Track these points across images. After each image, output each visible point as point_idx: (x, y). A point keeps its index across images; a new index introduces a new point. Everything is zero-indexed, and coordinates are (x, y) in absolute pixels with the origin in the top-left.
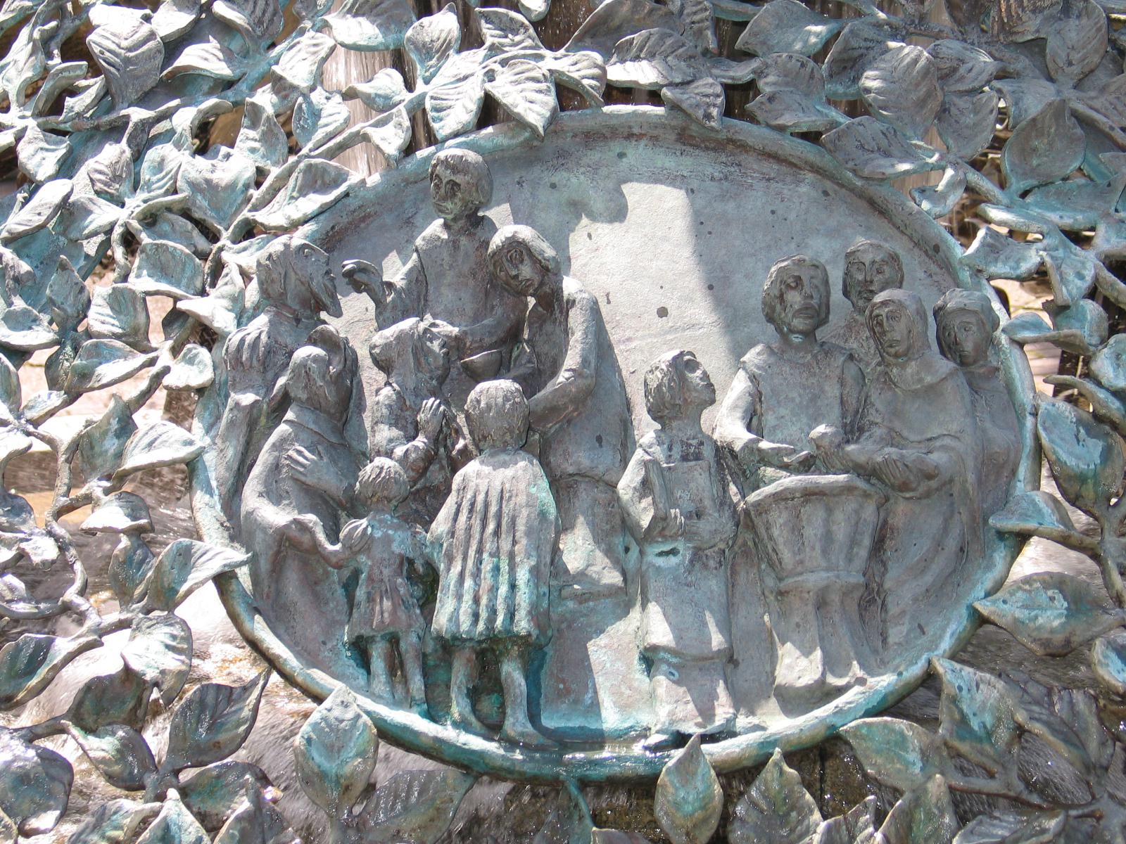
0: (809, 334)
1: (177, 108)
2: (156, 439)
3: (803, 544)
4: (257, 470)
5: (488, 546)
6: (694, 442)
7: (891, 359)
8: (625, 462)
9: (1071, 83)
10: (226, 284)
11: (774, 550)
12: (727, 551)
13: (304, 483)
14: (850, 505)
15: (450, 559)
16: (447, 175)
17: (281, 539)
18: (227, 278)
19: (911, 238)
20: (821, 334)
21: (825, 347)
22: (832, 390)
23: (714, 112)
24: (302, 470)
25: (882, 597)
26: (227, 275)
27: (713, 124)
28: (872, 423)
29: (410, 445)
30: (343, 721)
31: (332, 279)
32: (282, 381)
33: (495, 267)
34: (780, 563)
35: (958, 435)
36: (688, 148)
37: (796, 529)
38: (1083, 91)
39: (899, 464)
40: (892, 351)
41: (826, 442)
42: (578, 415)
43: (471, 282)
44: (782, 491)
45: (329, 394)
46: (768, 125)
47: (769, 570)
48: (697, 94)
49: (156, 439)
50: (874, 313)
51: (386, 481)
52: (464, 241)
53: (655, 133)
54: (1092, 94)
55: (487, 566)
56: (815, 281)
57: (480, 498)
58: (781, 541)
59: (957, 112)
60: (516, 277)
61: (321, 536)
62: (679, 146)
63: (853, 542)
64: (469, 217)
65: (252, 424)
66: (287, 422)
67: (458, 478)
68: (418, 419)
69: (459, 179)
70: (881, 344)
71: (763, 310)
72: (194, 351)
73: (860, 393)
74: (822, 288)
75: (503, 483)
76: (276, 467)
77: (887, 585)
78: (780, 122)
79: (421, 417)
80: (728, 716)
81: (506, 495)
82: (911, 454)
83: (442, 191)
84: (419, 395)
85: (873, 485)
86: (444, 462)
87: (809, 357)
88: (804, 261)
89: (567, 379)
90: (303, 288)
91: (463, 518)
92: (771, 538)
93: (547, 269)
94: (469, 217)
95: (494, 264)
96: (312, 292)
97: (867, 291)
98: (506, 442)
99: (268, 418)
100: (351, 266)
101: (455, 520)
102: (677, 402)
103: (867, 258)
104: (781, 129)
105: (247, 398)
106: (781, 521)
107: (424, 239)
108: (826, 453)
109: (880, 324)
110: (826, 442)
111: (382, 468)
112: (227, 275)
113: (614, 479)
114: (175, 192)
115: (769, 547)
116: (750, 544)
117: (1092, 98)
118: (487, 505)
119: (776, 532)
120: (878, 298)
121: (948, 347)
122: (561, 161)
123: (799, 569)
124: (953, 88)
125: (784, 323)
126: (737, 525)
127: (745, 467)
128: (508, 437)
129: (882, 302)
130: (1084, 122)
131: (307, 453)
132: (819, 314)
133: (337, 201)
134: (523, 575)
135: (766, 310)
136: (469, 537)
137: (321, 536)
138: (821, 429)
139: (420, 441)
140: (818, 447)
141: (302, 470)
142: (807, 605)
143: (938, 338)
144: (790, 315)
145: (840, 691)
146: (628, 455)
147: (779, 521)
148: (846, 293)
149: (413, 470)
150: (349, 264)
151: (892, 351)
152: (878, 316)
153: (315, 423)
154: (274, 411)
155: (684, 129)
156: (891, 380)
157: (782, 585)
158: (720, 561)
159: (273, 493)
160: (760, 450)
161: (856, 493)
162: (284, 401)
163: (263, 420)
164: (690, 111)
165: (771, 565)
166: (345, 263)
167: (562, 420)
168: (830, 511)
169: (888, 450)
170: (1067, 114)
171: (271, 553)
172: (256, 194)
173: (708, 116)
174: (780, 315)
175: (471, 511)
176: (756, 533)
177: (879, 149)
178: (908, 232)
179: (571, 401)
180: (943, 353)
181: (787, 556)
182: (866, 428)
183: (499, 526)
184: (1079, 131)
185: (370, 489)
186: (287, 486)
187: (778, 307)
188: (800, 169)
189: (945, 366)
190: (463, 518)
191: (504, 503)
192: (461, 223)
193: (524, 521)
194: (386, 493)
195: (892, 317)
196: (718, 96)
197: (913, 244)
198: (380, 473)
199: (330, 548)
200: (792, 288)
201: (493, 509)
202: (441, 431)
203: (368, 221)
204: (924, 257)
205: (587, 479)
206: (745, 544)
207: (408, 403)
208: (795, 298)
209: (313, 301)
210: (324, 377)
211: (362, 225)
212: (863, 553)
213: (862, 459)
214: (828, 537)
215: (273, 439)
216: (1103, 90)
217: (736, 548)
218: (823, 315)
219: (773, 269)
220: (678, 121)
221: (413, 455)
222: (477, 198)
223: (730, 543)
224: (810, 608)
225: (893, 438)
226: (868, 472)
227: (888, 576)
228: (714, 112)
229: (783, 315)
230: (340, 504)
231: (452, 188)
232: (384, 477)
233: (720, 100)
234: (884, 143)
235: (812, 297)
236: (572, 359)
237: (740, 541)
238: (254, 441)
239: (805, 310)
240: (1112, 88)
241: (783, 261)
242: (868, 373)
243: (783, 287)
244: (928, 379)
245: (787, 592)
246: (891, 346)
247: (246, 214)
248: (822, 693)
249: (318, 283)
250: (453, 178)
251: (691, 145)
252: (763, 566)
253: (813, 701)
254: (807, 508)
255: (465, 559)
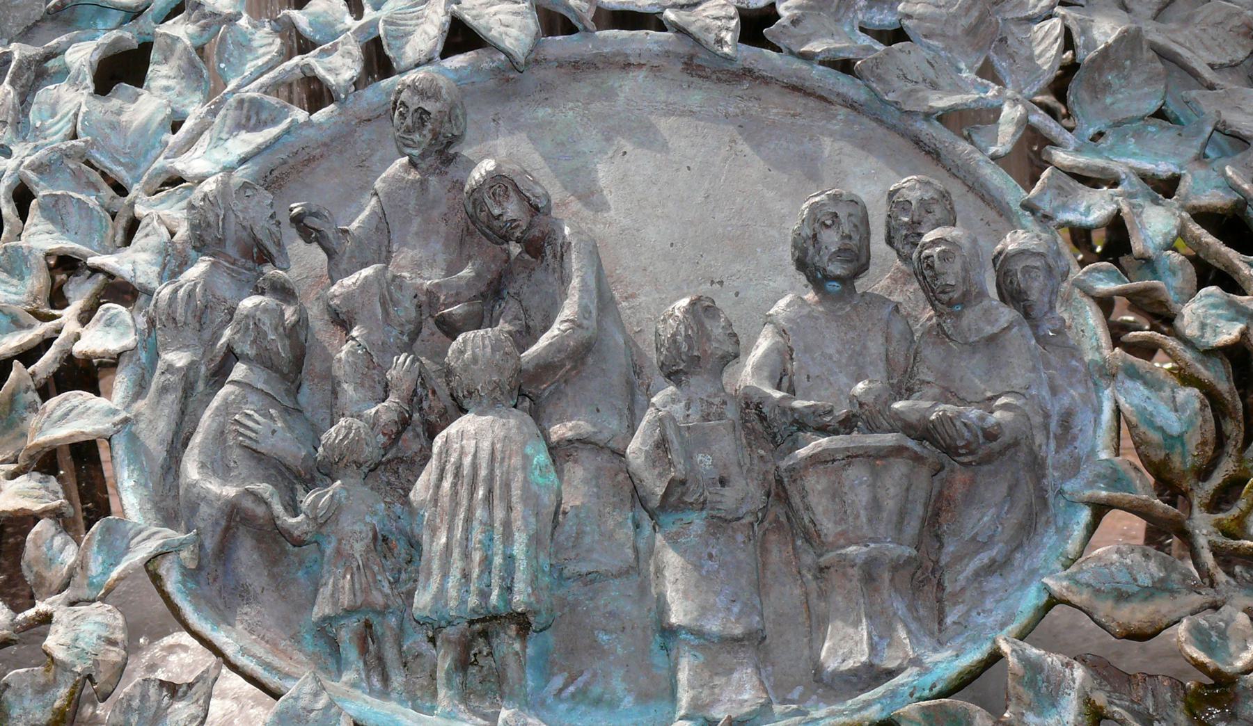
0: (847, 281)
1: (70, 43)
2: (71, 411)
3: (845, 512)
4: (197, 439)
5: (479, 513)
6: (717, 401)
7: (944, 307)
8: (632, 429)
9: (1150, 13)
10: (147, 235)
11: (812, 521)
12: (756, 525)
13: (255, 451)
14: (899, 468)
15: (434, 531)
16: (415, 102)
17: (232, 512)
18: (149, 229)
19: (964, 183)
20: (861, 285)
21: (867, 298)
22: (875, 346)
23: (728, 37)
24: (253, 435)
25: (937, 576)
26: (148, 225)
27: (726, 50)
28: (923, 382)
29: (379, 406)
30: (313, 710)
31: (279, 223)
32: (227, 333)
33: (474, 207)
34: (819, 536)
35: (1023, 391)
36: (696, 79)
37: (836, 494)
38: (1163, 22)
39: (958, 423)
40: (945, 297)
41: (870, 399)
42: (577, 373)
43: (443, 228)
44: (820, 452)
45: (282, 348)
46: (791, 53)
47: (806, 546)
48: (707, 17)
49: (71, 411)
50: (923, 255)
51: (357, 441)
52: (433, 180)
53: (656, 62)
54: (1173, 26)
55: (477, 535)
56: (853, 219)
57: (467, 461)
58: (819, 510)
59: (1016, 44)
60: (498, 217)
61: (278, 509)
62: (686, 77)
63: (902, 514)
64: (440, 152)
65: (188, 389)
66: (233, 382)
67: (439, 441)
68: (389, 377)
69: (429, 106)
70: (933, 291)
71: (793, 255)
72: (112, 311)
73: (908, 350)
74: (862, 229)
75: (493, 444)
76: (220, 435)
77: (944, 560)
78: (805, 48)
79: (392, 374)
80: (762, 701)
81: (498, 455)
82: (973, 413)
83: (409, 121)
84: (388, 350)
85: (925, 447)
86: (420, 430)
87: (848, 308)
88: (841, 195)
89: (565, 331)
90: (245, 234)
91: (447, 484)
92: (808, 508)
93: (537, 209)
94: (440, 152)
95: (474, 203)
96: (255, 238)
97: (915, 231)
98: (495, 398)
99: (207, 384)
100: (300, 208)
101: (438, 486)
102: (696, 354)
103: (914, 196)
104: (807, 57)
105: (179, 358)
106: (819, 487)
107: (384, 181)
108: (870, 412)
109: (931, 267)
110: (870, 399)
111: (350, 428)
112: (148, 225)
113: (621, 446)
114: (75, 136)
115: (806, 520)
116: (783, 519)
117: (1173, 31)
118: (475, 467)
119: (813, 500)
120: (929, 237)
121: (1012, 294)
122: (544, 95)
123: (842, 541)
124: (1009, 16)
125: (817, 269)
126: (768, 495)
127: (776, 430)
128: (497, 394)
129: (932, 242)
130: (1164, 55)
131: (256, 416)
132: (859, 261)
133: (277, 139)
134: (519, 549)
135: (797, 254)
136: (455, 503)
137: (278, 509)
138: (860, 387)
139: (393, 400)
140: (861, 405)
141: (253, 435)
142: (851, 581)
143: (998, 286)
144: (826, 258)
145: (891, 674)
146: (636, 423)
147: (815, 483)
148: (890, 241)
149: (384, 434)
150: (297, 208)
151: (945, 297)
152: (928, 257)
153: (266, 382)
154: (214, 374)
155: (691, 57)
156: (945, 333)
157: (822, 559)
158: (749, 536)
159: (217, 466)
160: (793, 410)
161: (906, 454)
162: (231, 356)
163: (201, 386)
164: (701, 35)
165: (808, 539)
166: (292, 205)
167: (558, 381)
168: (875, 474)
169: (942, 407)
170: (1145, 47)
171: (219, 529)
172: (172, 139)
173: (720, 41)
174: (813, 258)
175: (457, 475)
176: (790, 505)
177: (924, 80)
178: (961, 174)
179: (568, 357)
180: (1003, 299)
181: (828, 527)
182: (916, 388)
183: (490, 491)
184: (1159, 66)
185: (337, 453)
186: (236, 454)
187: (811, 250)
188: (831, 103)
189: (1007, 314)
190: (447, 484)
191: (497, 465)
192: (431, 160)
193: (520, 484)
194: (355, 457)
195: (944, 256)
196: (732, 18)
197: (967, 188)
198: (348, 434)
199: (293, 520)
200: (828, 227)
201: (483, 472)
202: (415, 391)
203: (313, 165)
204: (979, 202)
205: (589, 446)
206: (777, 520)
207: (375, 360)
208: (831, 240)
209: (255, 250)
210: (276, 329)
211: (307, 170)
212: (912, 527)
213: (913, 418)
214: (875, 505)
215: (216, 402)
216: (1187, 21)
217: (766, 524)
218: (863, 260)
219: (805, 206)
220: (684, 48)
221: (384, 417)
222: (448, 130)
223: (760, 515)
224: (856, 583)
225: (948, 394)
226: (924, 432)
227: (945, 551)
228: (728, 37)
229: (817, 258)
230: (298, 477)
231: (421, 118)
232: (353, 439)
233: (733, 23)
234: (931, 73)
235: (850, 237)
236: (569, 310)
237: (771, 517)
238: (190, 409)
239: (843, 253)
240: (1198, 19)
241: (816, 196)
242: (916, 330)
243: (817, 225)
244: (989, 330)
245: (828, 568)
246: (943, 292)
247: (160, 162)
248: (874, 675)
249: (262, 228)
250: (422, 105)
251: (700, 76)
252: (799, 542)
253: (860, 686)
254: (849, 472)
255: (450, 530)
